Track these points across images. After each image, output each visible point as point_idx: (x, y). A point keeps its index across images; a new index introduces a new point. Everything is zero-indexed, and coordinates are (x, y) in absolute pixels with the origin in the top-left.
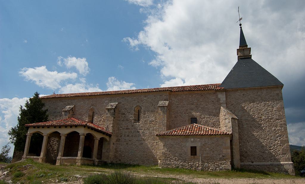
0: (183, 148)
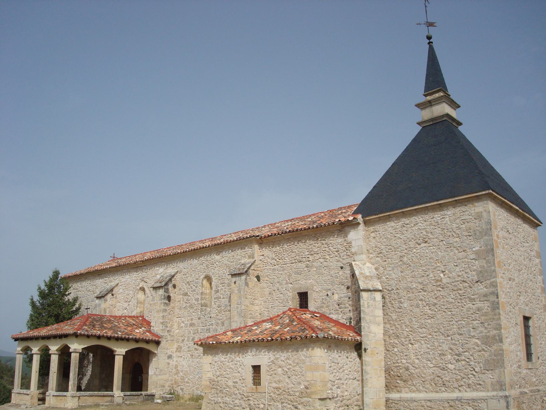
0: (240, 369)
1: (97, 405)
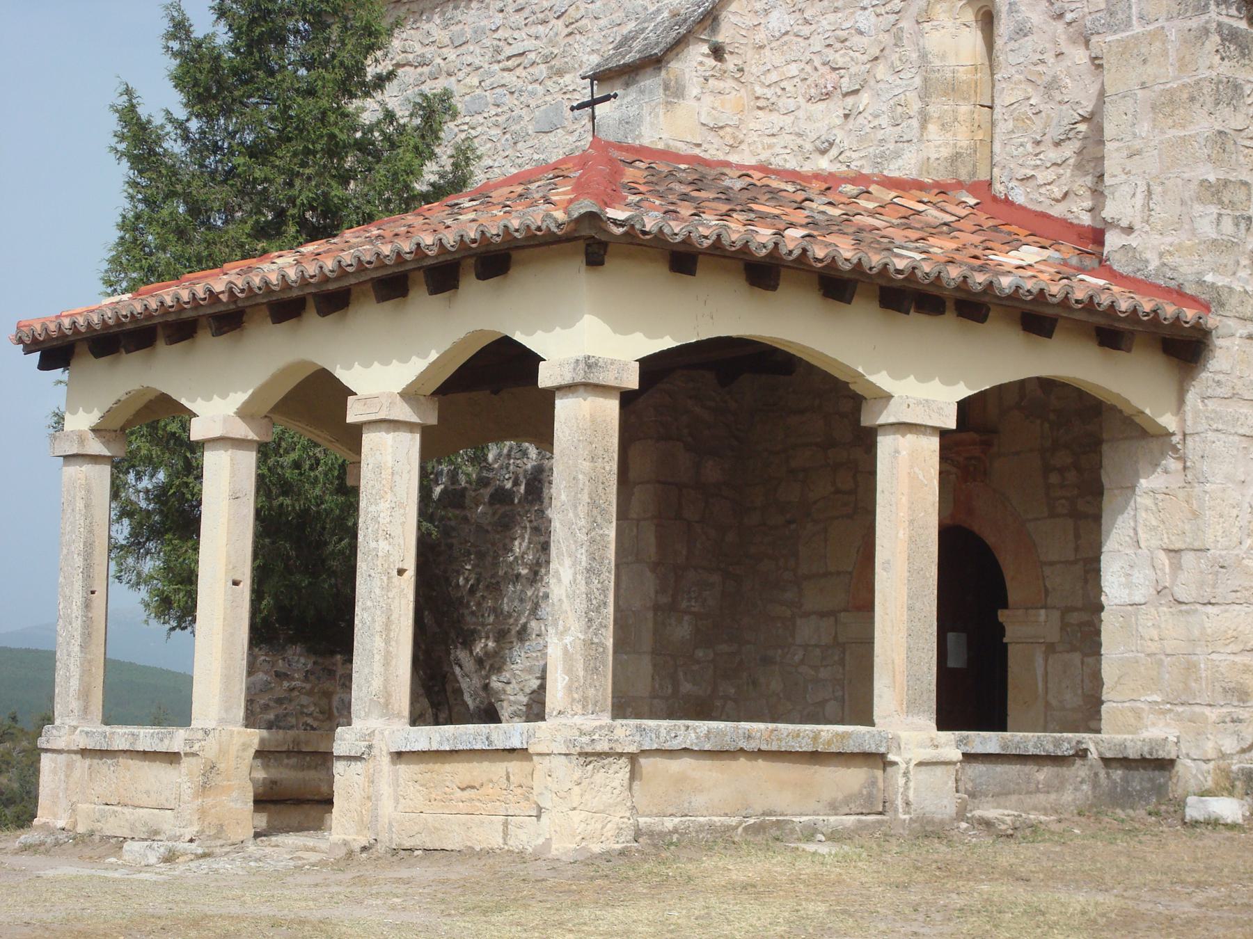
1: (770, 832)
